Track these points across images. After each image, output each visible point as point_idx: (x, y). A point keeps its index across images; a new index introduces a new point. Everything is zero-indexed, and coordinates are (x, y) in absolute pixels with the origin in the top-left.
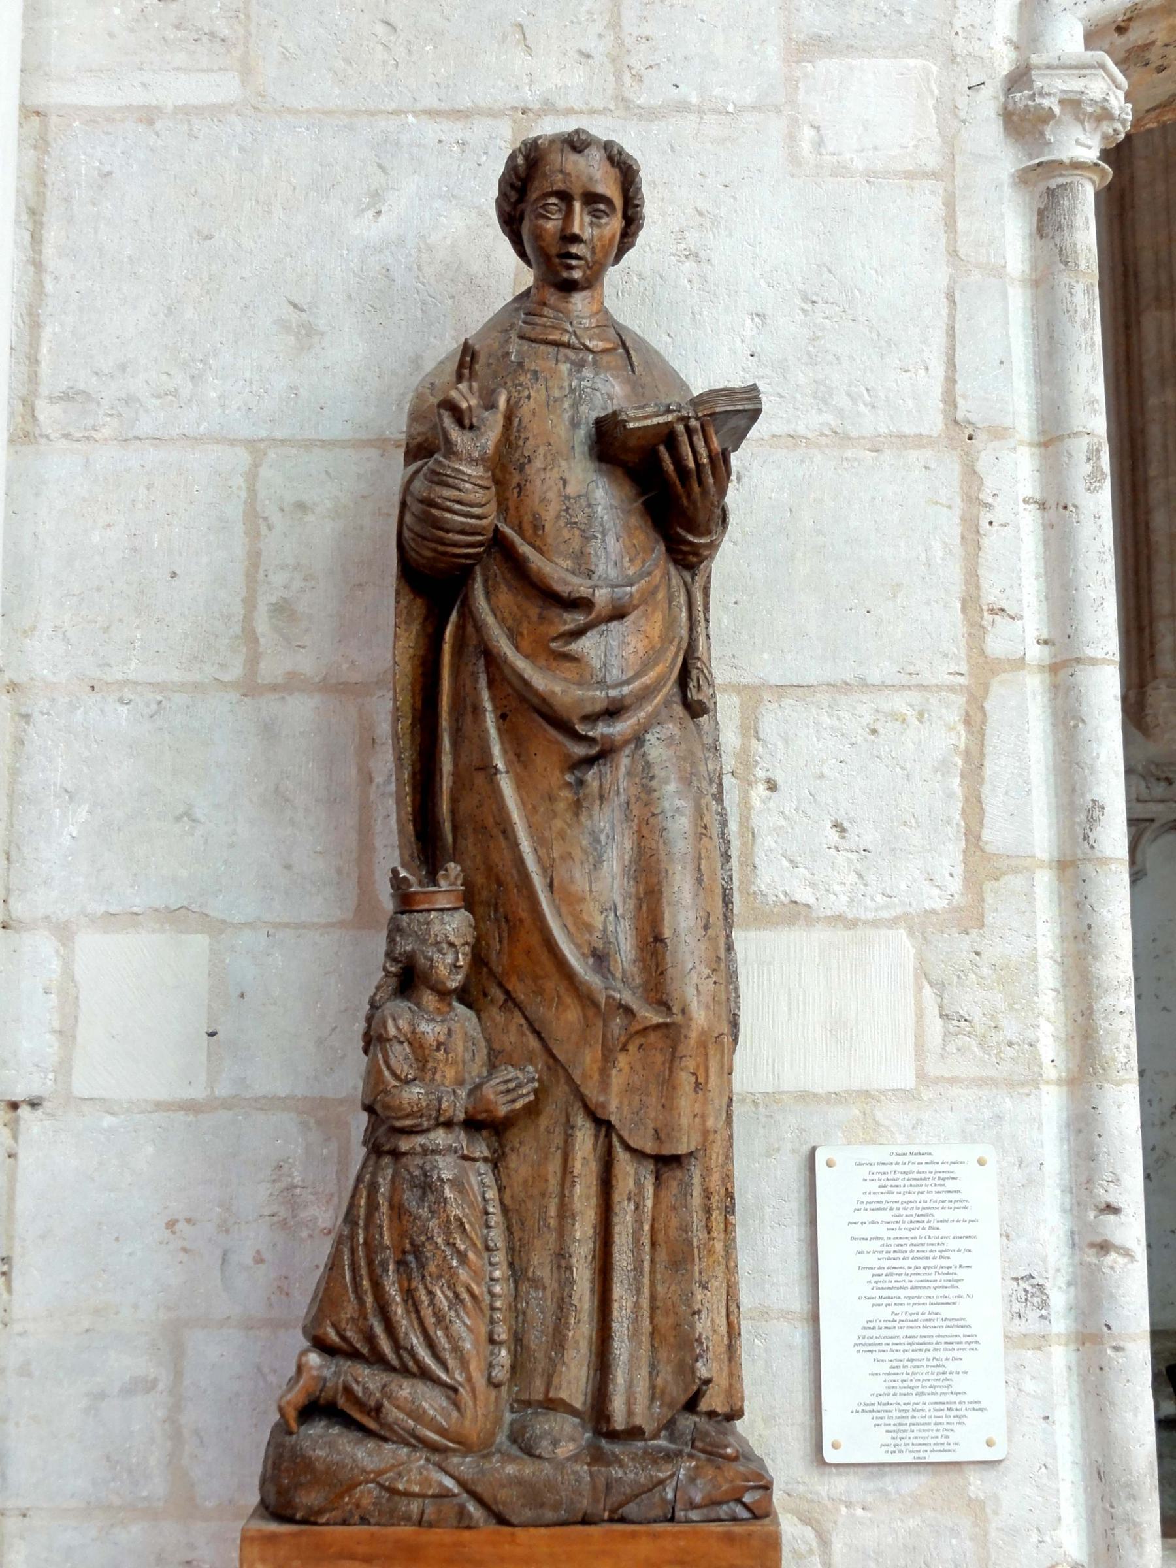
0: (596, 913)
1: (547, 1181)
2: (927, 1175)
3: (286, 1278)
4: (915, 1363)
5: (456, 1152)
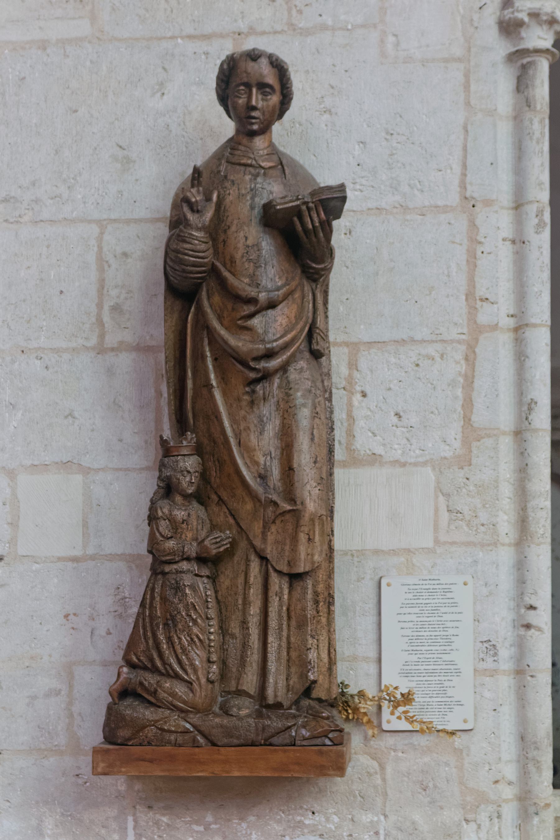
0: (261, 456)
1: (238, 587)
2: (438, 590)
3: (122, 641)
4: (429, 682)
5: (192, 573)
